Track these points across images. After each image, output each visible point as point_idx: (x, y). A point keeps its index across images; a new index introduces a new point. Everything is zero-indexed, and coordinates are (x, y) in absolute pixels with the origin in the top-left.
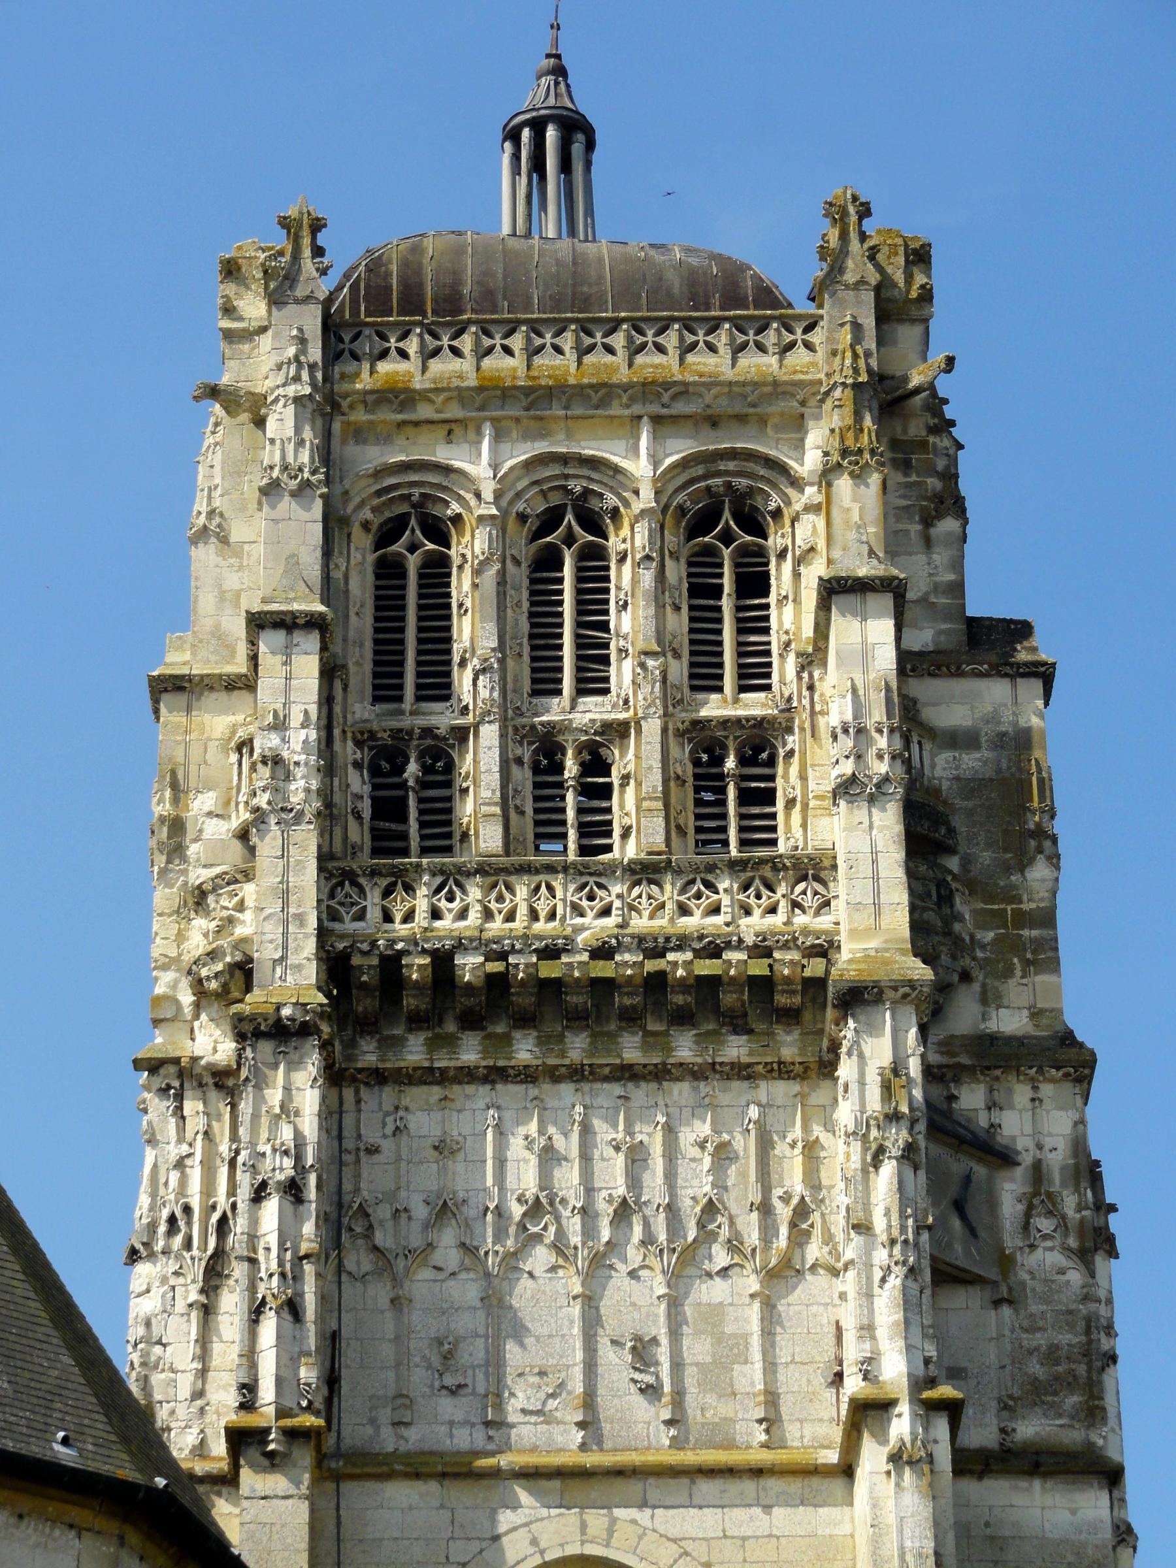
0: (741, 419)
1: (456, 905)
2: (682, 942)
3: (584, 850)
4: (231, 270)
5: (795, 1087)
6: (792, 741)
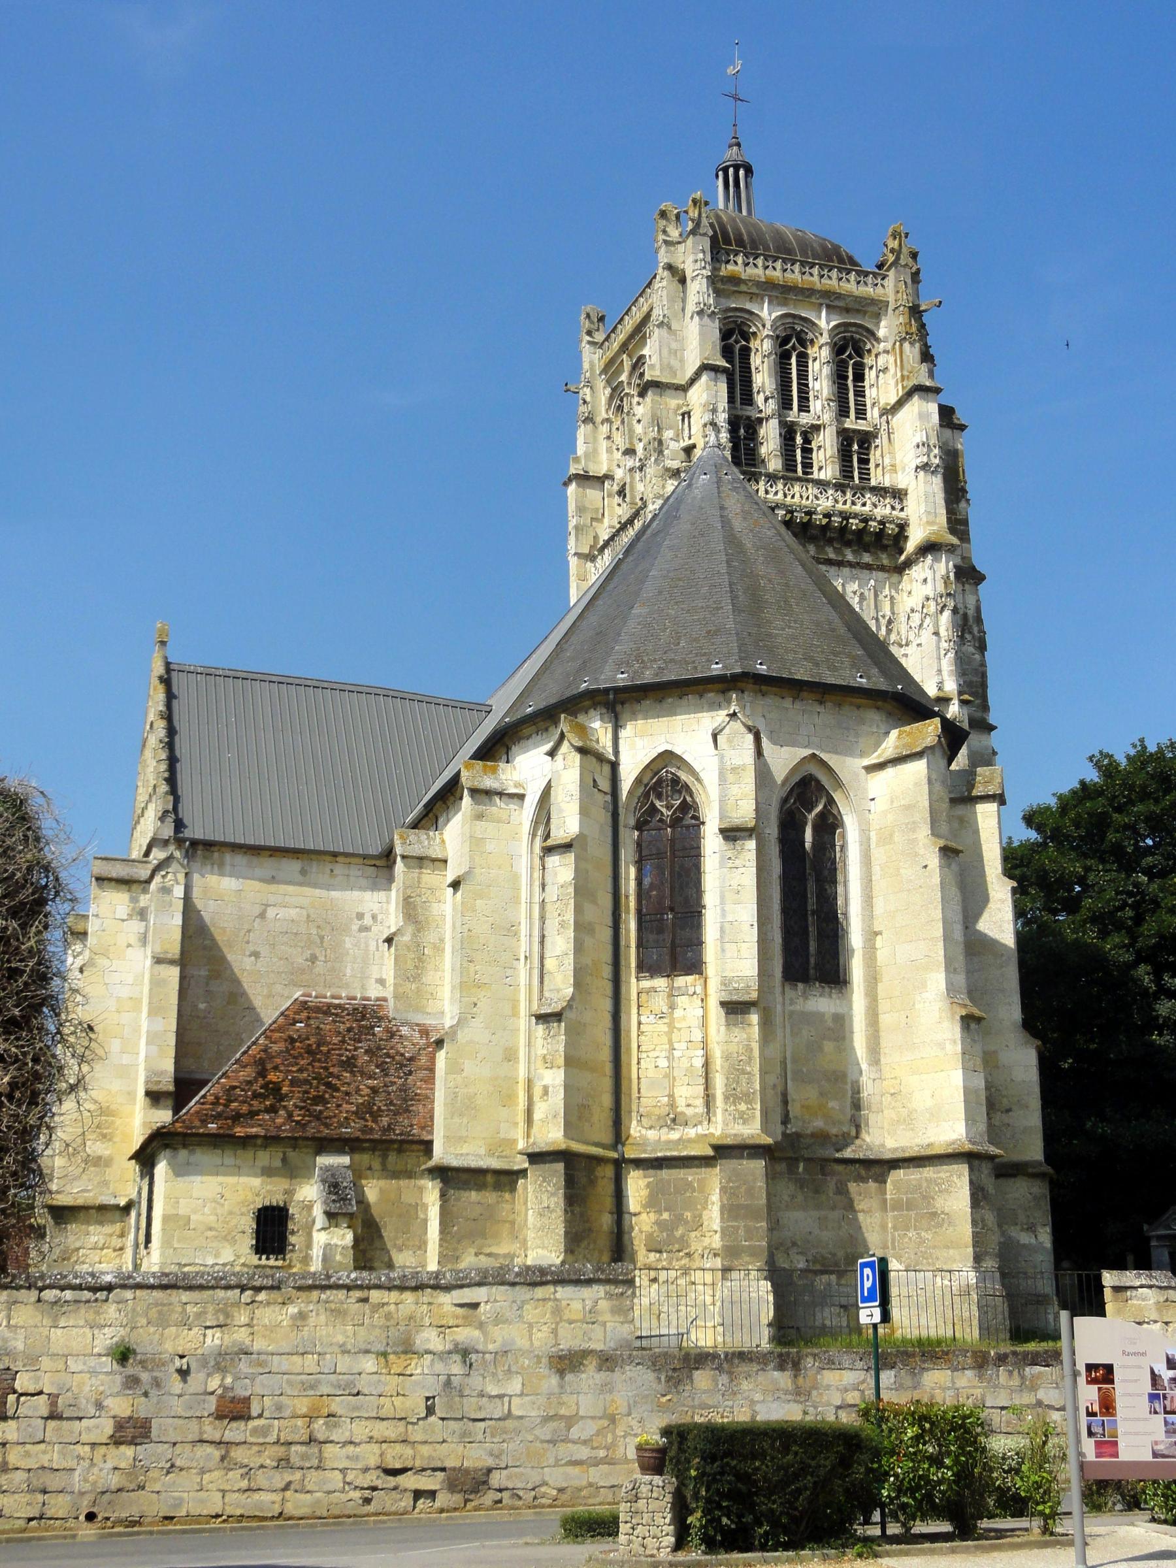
0: (858, 311)
1: (774, 489)
2: (856, 516)
3: (805, 473)
4: (663, 214)
5: (886, 575)
6: (878, 441)
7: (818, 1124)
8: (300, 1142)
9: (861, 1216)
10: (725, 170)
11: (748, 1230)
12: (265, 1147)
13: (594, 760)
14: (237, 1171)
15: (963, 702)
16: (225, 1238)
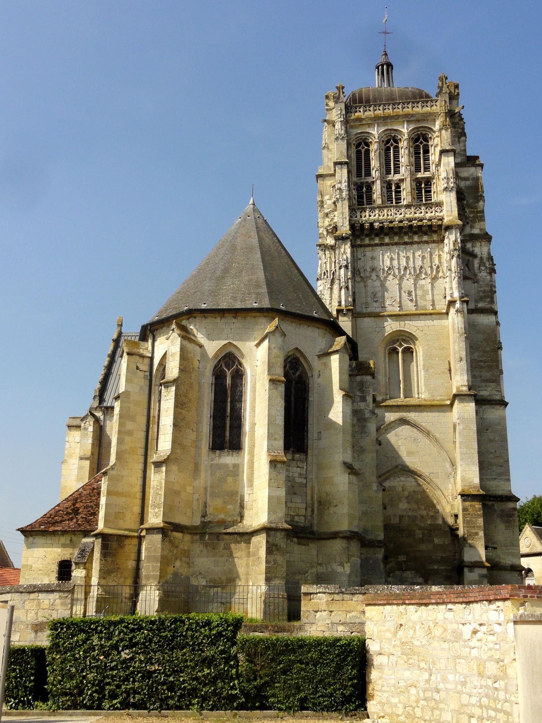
0: (424, 120)
3: (396, 203)
4: (327, 97)
5: (436, 245)
6: (434, 181)
7: (222, 516)
8: (76, 532)
9: (236, 560)
10: (378, 68)
11: (153, 567)
12: (63, 535)
13: (138, 357)
14: (52, 545)
15: (463, 302)
16: (46, 574)
